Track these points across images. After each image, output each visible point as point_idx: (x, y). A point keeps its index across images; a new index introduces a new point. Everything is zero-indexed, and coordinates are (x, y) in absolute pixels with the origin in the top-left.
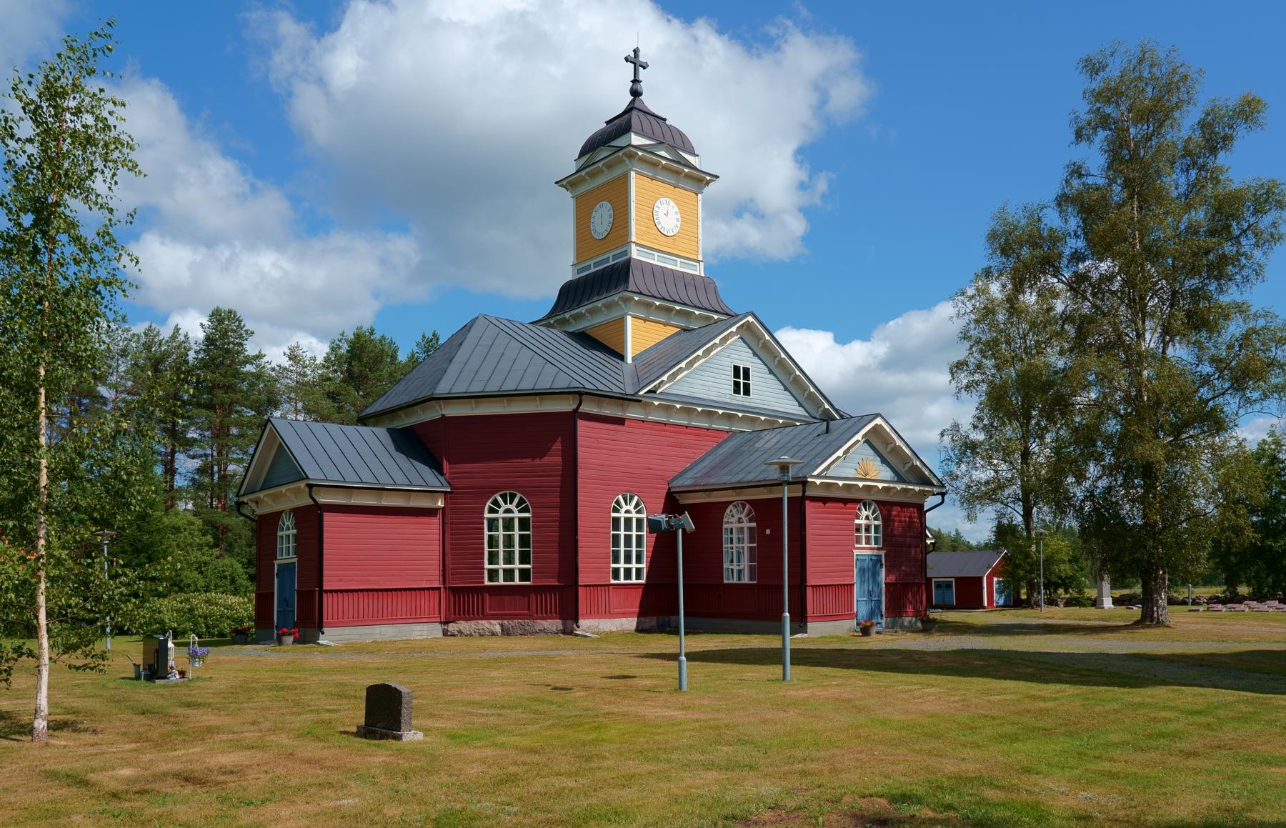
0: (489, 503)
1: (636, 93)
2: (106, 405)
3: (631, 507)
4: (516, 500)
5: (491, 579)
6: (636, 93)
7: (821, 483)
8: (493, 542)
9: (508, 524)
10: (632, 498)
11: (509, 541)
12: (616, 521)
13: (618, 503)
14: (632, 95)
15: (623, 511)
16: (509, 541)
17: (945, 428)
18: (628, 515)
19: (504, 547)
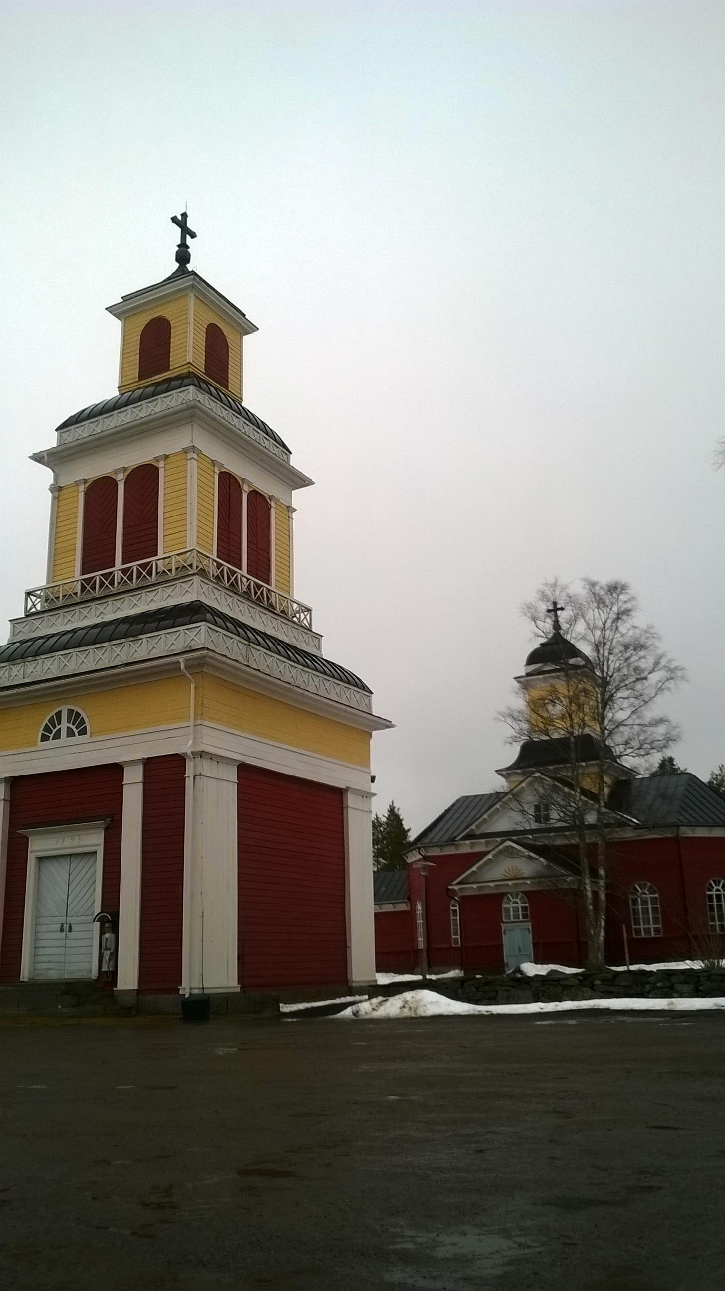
0: (717, 879)
1: (183, 256)
2: (595, 845)
3: (720, 888)
4: (519, 897)
5: (636, 934)
6: (183, 256)
7: (477, 887)
8: (635, 912)
9: (645, 902)
10: (719, 882)
11: (646, 911)
12: (710, 896)
13: (710, 885)
14: (177, 260)
15: (714, 890)
16: (646, 911)
17: (670, 718)
18: (718, 892)
19: (716, 902)
